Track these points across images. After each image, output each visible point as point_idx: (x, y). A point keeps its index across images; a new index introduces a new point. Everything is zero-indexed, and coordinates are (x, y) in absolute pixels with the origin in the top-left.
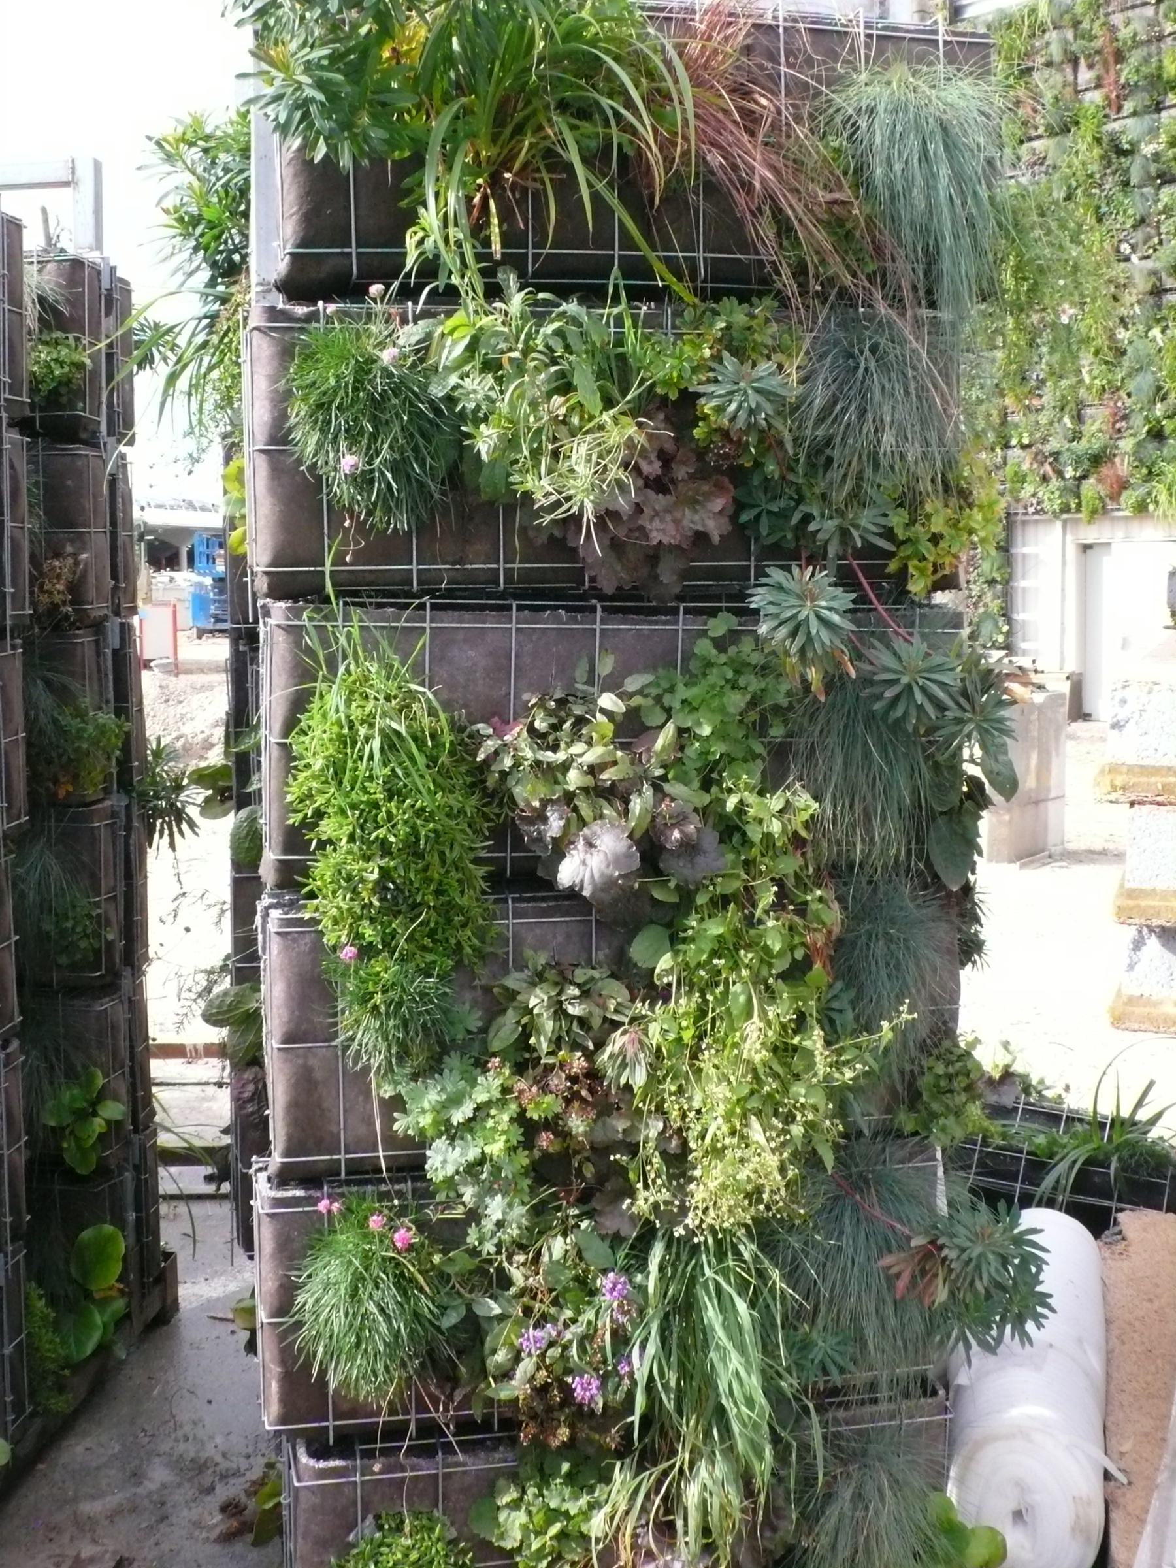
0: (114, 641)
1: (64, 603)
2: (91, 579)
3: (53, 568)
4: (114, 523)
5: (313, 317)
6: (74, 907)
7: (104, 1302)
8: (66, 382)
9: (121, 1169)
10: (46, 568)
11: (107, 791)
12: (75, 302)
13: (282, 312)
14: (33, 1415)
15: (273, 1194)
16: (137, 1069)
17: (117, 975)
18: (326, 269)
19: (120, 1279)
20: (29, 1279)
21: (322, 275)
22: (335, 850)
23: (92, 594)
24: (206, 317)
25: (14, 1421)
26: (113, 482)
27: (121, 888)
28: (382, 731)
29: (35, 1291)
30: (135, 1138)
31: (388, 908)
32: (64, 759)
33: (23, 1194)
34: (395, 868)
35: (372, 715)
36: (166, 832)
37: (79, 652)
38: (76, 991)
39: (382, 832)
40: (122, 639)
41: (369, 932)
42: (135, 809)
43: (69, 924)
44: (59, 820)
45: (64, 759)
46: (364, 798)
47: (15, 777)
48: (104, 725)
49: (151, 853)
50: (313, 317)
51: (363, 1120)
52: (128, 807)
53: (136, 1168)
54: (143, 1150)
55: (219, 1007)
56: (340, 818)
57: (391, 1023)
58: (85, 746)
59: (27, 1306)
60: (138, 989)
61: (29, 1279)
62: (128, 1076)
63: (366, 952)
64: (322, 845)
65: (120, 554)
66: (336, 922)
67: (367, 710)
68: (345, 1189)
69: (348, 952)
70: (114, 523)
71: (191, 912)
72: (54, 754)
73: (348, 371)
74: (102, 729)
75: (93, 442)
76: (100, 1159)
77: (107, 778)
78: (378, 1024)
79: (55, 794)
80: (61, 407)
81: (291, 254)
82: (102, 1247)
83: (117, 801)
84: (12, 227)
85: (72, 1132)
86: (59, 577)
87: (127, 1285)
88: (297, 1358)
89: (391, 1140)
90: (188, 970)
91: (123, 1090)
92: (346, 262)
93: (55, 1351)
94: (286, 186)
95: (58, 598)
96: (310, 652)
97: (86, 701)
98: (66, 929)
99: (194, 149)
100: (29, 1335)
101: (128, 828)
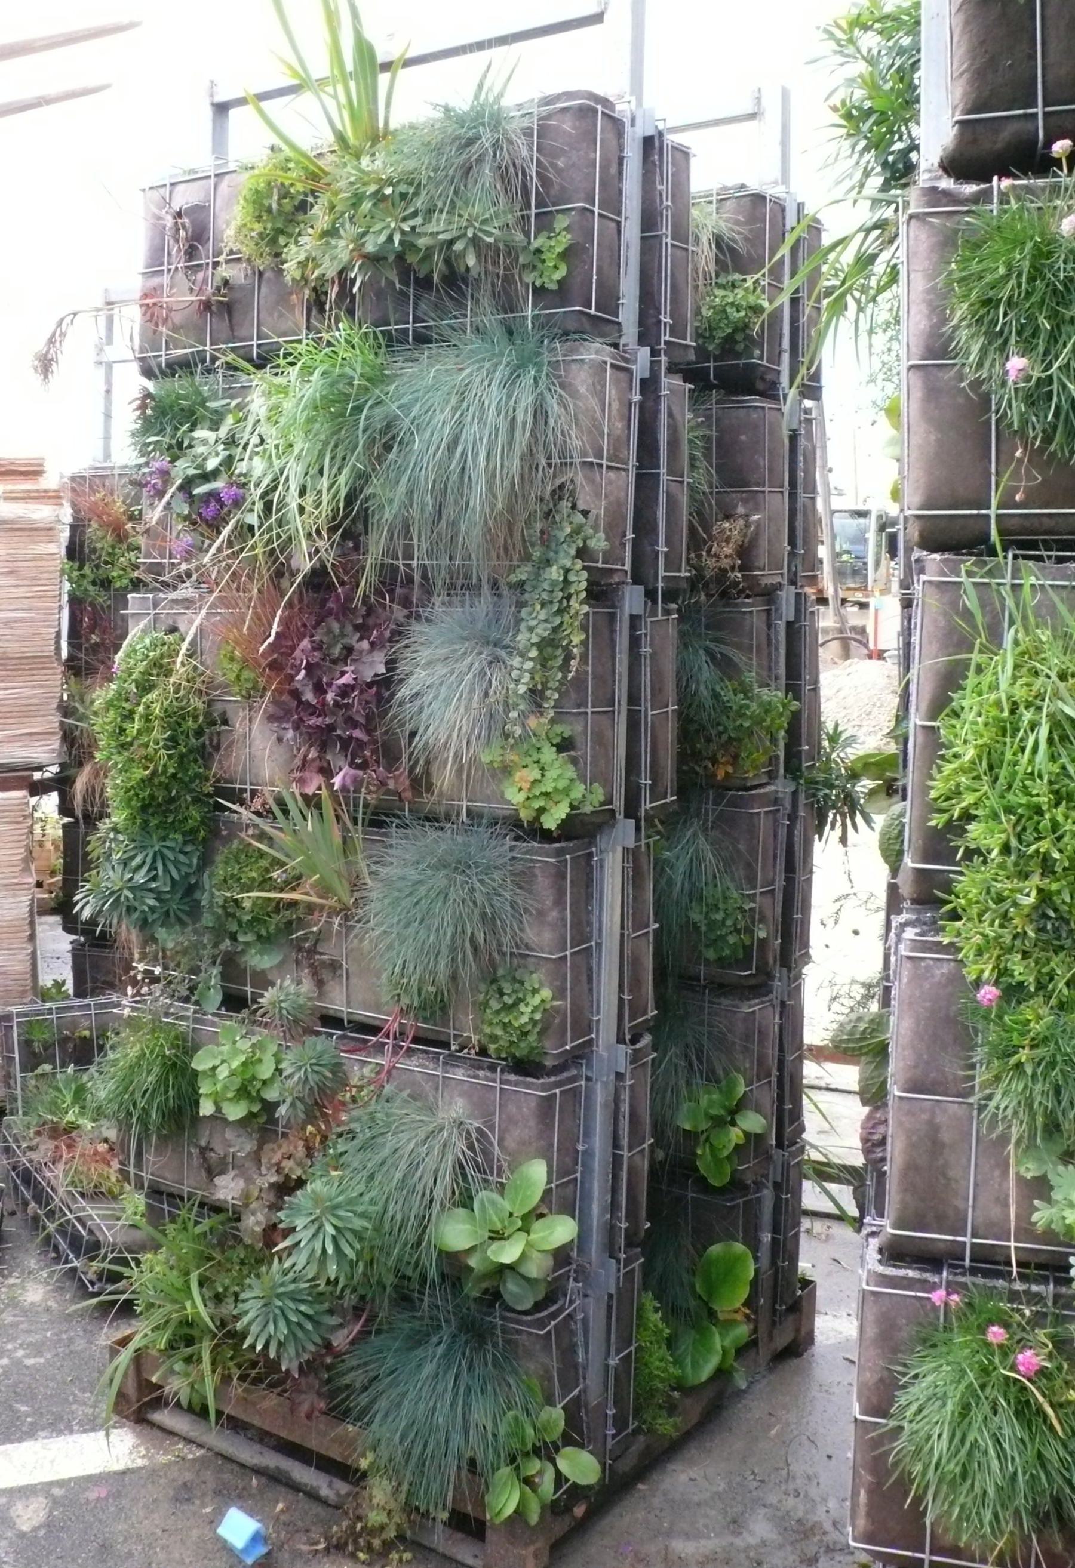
0: (787, 611)
1: (733, 568)
2: (764, 544)
3: (723, 531)
4: (793, 484)
5: (984, 197)
6: (725, 898)
7: (728, 1325)
8: (743, 327)
9: (759, 1186)
10: (715, 530)
11: (772, 776)
12: (755, 239)
13: (945, 193)
14: (636, 1432)
15: (881, 1269)
16: (787, 1080)
17: (770, 976)
18: (1006, 135)
19: (747, 1303)
20: (645, 1287)
21: (999, 146)
22: (985, 862)
23: (763, 560)
24: (876, 227)
25: (614, 1436)
26: (794, 437)
27: (780, 883)
28: (1051, 716)
29: (649, 1301)
30: (777, 1154)
31: (1047, 942)
32: (725, 737)
33: (643, 1199)
34: (1059, 892)
35: (1041, 696)
36: (839, 824)
37: (748, 622)
38: (723, 988)
39: (1044, 846)
40: (798, 610)
41: (1018, 968)
42: (802, 797)
43: (719, 916)
44: (716, 803)
45: (725, 737)
46: (1024, 800)
47: (661, 753)
48: (770, 703)
49: (818, 846)
50: (984, 197)
51: (997, 1199)
52: (795, 793)
53: (777, 1186)
54: (786, 1167)
55: (851, 1033)
56: (991, 823)
57: (1039, 1087)
58: (746, 724)
59: (640, 1317)
60: (795, 991)
61: (645, 1287)
62: (774, 1085)
63: (1014, 993)
64: (969, 854)
65: (800, 517)
66: (980, 953)
67: (1035, 688)
68: (967, 1279)
69: (988, 993)
70: (793, 484)
71: (853, 915)
72: (713, 732)
73: (1022, 259)
74: (767, 708)
75: (771, 392)
76: (734, 1172)
77: (773, 760)
78: (1020, 1087)
79: (714, 775)
80: (738, 355)
81: (957, 122)
82: (732, 1264)
83: (782, 787)
84: (678, 155)
85: (707, 1139)
86: (728, 540)
87: (756, 1312)
88: (889, 1473)
89: (1026, 1231)
90: (843, 979)
91: (767, 1098)
92: (1029, 126)
93: (665, 1370)
94: (955, 39)
95: (725, 563)
96: (967, 615)
97: (751, 677)
98: (715, 921)
99: (870, 33)
100: (639, 1349)
101: (793, 817)
